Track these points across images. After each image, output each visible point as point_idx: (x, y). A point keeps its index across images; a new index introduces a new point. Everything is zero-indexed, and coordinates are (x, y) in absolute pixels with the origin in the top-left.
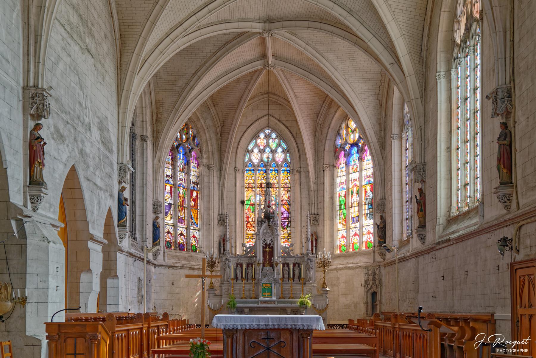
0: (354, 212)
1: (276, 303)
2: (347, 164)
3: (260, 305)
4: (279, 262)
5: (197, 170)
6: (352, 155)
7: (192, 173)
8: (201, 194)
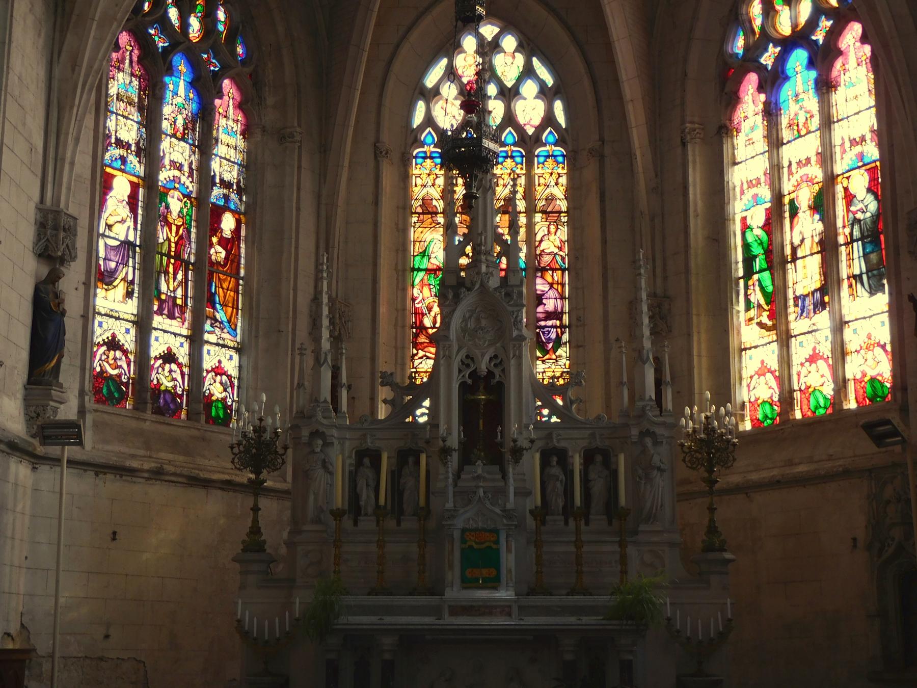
0: (805, 276)
1: (515, 610)
2: (771, 112)
3: (449, 620)
4: (525, 444)
6: (787, 78)
7: (221, 150)
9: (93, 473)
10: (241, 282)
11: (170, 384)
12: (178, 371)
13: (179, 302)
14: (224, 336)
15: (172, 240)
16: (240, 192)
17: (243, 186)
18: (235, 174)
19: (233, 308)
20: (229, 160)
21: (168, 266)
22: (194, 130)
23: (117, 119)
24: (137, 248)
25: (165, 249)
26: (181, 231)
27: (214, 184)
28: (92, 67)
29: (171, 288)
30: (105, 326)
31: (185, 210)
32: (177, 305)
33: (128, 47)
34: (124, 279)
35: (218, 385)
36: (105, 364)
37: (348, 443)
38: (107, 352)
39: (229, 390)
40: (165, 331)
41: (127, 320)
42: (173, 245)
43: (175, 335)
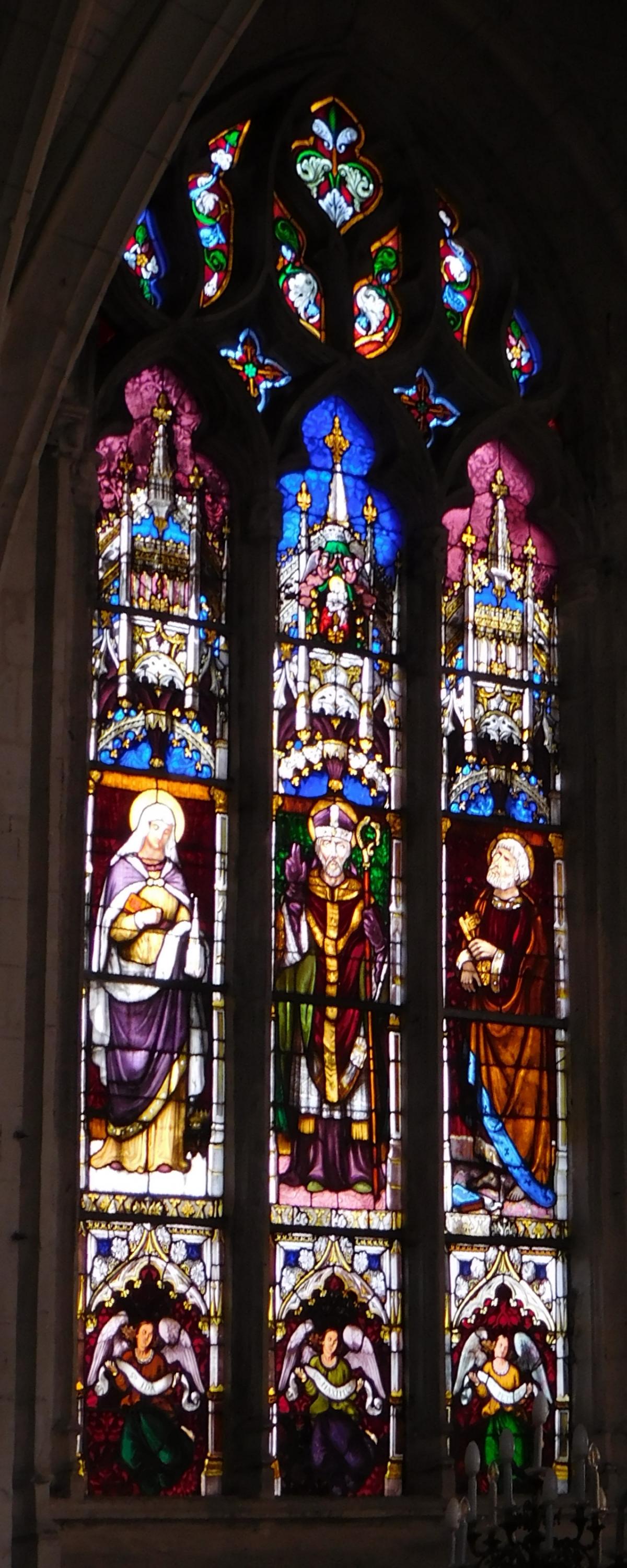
10: (561, 1035)
11: (342, 1393)
12: (368, 1346)
13: (360, 1132)
14: (512, 1209)
15: (330, 950)
16: (542, 766)
18: (525, 715)
19: (537, 1119)
20: (503, 680)
21: (318, 1030)
22: (384, 612)
23: (132, 626)
24: (216, 996)
25: (306, 982)
26: (356, 918)
27: (458, 758)
29: (333, 1095)
30: (119, 1250)
31: (367, 853)
33: (159, 413)
34: (178, 1097)
35: (501, 1366)
36: (311, 1372)
39: (540, 1374)
40: (318, 1232)
41: (190, 1220)
42: (332, 964)
43: (352, 1235)
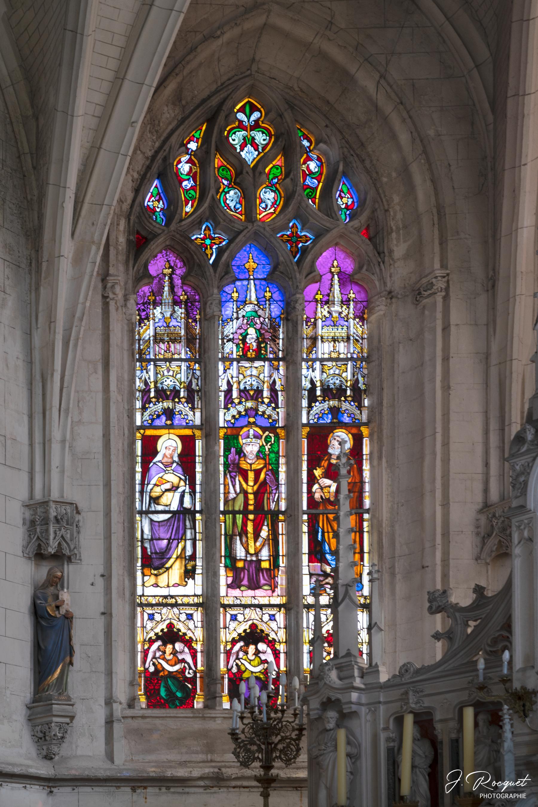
5: (356, 328)
8: (377, 438)
9: (128, 789)
12: (269, 651)
13: (265, 565)
15: (250, 490)
17: (363, 387)
21: (244, 524)
22: (274, 338)
26: (262, 476)
28: (74, 316)
29: (252, 551)
30: (157, 617)
32: (262, 570)
36: (161, 661)
37: (382, 707)
38: (162, 648)
42: (251, 497)
